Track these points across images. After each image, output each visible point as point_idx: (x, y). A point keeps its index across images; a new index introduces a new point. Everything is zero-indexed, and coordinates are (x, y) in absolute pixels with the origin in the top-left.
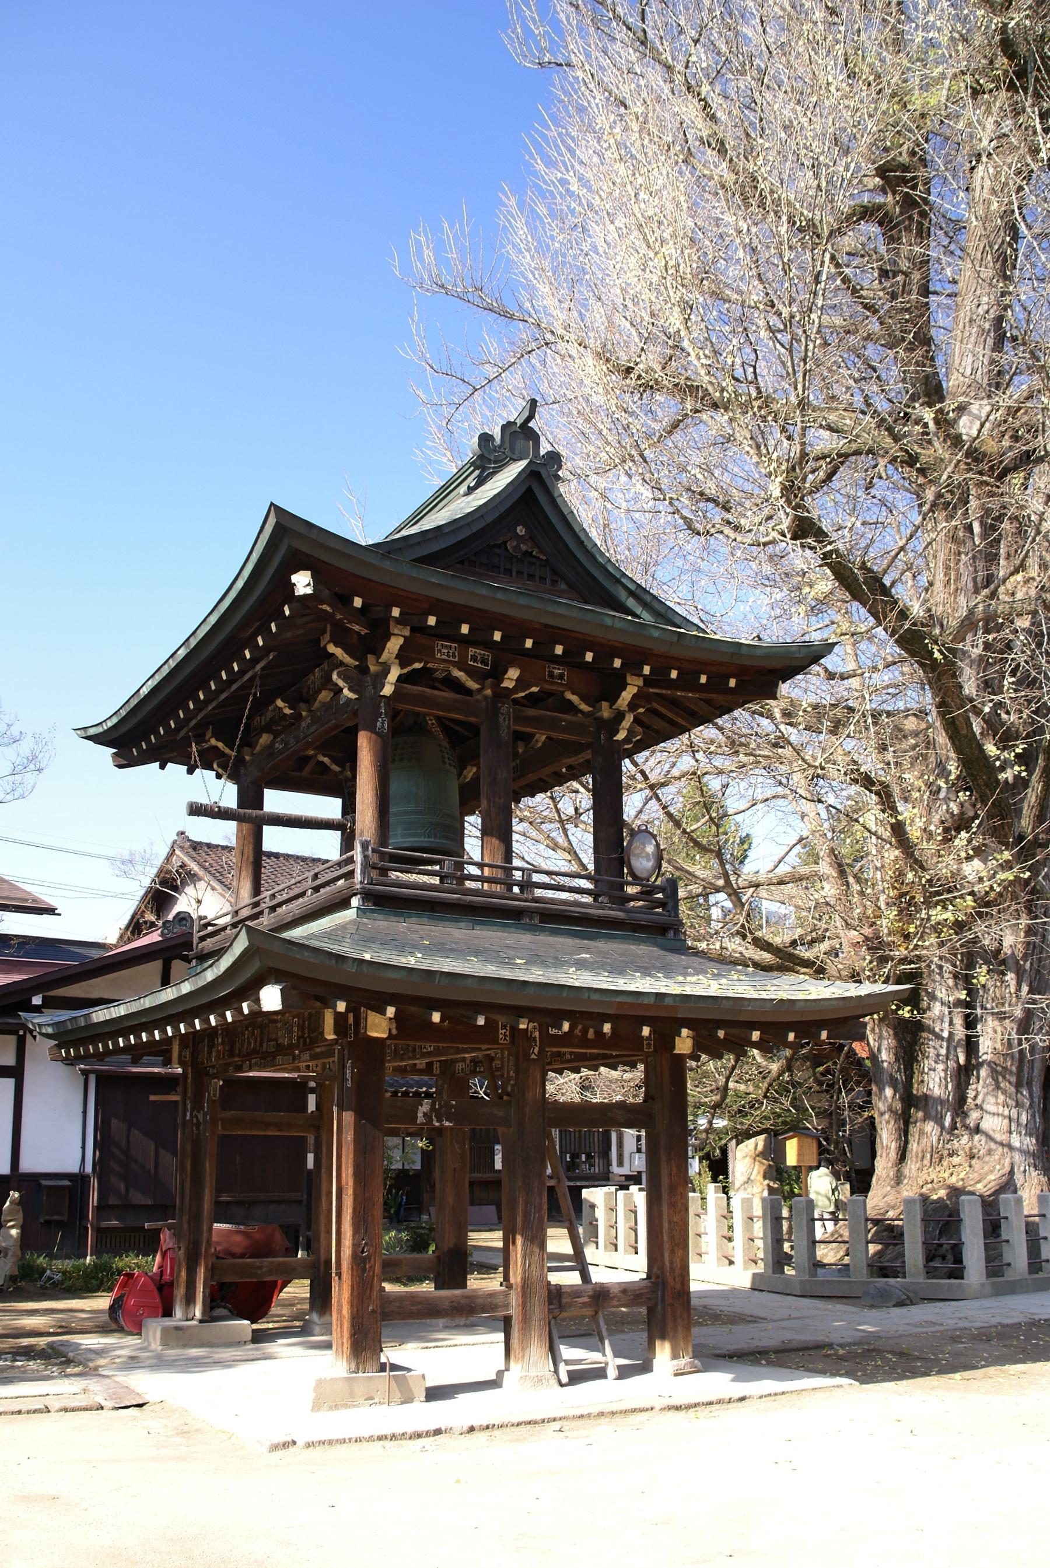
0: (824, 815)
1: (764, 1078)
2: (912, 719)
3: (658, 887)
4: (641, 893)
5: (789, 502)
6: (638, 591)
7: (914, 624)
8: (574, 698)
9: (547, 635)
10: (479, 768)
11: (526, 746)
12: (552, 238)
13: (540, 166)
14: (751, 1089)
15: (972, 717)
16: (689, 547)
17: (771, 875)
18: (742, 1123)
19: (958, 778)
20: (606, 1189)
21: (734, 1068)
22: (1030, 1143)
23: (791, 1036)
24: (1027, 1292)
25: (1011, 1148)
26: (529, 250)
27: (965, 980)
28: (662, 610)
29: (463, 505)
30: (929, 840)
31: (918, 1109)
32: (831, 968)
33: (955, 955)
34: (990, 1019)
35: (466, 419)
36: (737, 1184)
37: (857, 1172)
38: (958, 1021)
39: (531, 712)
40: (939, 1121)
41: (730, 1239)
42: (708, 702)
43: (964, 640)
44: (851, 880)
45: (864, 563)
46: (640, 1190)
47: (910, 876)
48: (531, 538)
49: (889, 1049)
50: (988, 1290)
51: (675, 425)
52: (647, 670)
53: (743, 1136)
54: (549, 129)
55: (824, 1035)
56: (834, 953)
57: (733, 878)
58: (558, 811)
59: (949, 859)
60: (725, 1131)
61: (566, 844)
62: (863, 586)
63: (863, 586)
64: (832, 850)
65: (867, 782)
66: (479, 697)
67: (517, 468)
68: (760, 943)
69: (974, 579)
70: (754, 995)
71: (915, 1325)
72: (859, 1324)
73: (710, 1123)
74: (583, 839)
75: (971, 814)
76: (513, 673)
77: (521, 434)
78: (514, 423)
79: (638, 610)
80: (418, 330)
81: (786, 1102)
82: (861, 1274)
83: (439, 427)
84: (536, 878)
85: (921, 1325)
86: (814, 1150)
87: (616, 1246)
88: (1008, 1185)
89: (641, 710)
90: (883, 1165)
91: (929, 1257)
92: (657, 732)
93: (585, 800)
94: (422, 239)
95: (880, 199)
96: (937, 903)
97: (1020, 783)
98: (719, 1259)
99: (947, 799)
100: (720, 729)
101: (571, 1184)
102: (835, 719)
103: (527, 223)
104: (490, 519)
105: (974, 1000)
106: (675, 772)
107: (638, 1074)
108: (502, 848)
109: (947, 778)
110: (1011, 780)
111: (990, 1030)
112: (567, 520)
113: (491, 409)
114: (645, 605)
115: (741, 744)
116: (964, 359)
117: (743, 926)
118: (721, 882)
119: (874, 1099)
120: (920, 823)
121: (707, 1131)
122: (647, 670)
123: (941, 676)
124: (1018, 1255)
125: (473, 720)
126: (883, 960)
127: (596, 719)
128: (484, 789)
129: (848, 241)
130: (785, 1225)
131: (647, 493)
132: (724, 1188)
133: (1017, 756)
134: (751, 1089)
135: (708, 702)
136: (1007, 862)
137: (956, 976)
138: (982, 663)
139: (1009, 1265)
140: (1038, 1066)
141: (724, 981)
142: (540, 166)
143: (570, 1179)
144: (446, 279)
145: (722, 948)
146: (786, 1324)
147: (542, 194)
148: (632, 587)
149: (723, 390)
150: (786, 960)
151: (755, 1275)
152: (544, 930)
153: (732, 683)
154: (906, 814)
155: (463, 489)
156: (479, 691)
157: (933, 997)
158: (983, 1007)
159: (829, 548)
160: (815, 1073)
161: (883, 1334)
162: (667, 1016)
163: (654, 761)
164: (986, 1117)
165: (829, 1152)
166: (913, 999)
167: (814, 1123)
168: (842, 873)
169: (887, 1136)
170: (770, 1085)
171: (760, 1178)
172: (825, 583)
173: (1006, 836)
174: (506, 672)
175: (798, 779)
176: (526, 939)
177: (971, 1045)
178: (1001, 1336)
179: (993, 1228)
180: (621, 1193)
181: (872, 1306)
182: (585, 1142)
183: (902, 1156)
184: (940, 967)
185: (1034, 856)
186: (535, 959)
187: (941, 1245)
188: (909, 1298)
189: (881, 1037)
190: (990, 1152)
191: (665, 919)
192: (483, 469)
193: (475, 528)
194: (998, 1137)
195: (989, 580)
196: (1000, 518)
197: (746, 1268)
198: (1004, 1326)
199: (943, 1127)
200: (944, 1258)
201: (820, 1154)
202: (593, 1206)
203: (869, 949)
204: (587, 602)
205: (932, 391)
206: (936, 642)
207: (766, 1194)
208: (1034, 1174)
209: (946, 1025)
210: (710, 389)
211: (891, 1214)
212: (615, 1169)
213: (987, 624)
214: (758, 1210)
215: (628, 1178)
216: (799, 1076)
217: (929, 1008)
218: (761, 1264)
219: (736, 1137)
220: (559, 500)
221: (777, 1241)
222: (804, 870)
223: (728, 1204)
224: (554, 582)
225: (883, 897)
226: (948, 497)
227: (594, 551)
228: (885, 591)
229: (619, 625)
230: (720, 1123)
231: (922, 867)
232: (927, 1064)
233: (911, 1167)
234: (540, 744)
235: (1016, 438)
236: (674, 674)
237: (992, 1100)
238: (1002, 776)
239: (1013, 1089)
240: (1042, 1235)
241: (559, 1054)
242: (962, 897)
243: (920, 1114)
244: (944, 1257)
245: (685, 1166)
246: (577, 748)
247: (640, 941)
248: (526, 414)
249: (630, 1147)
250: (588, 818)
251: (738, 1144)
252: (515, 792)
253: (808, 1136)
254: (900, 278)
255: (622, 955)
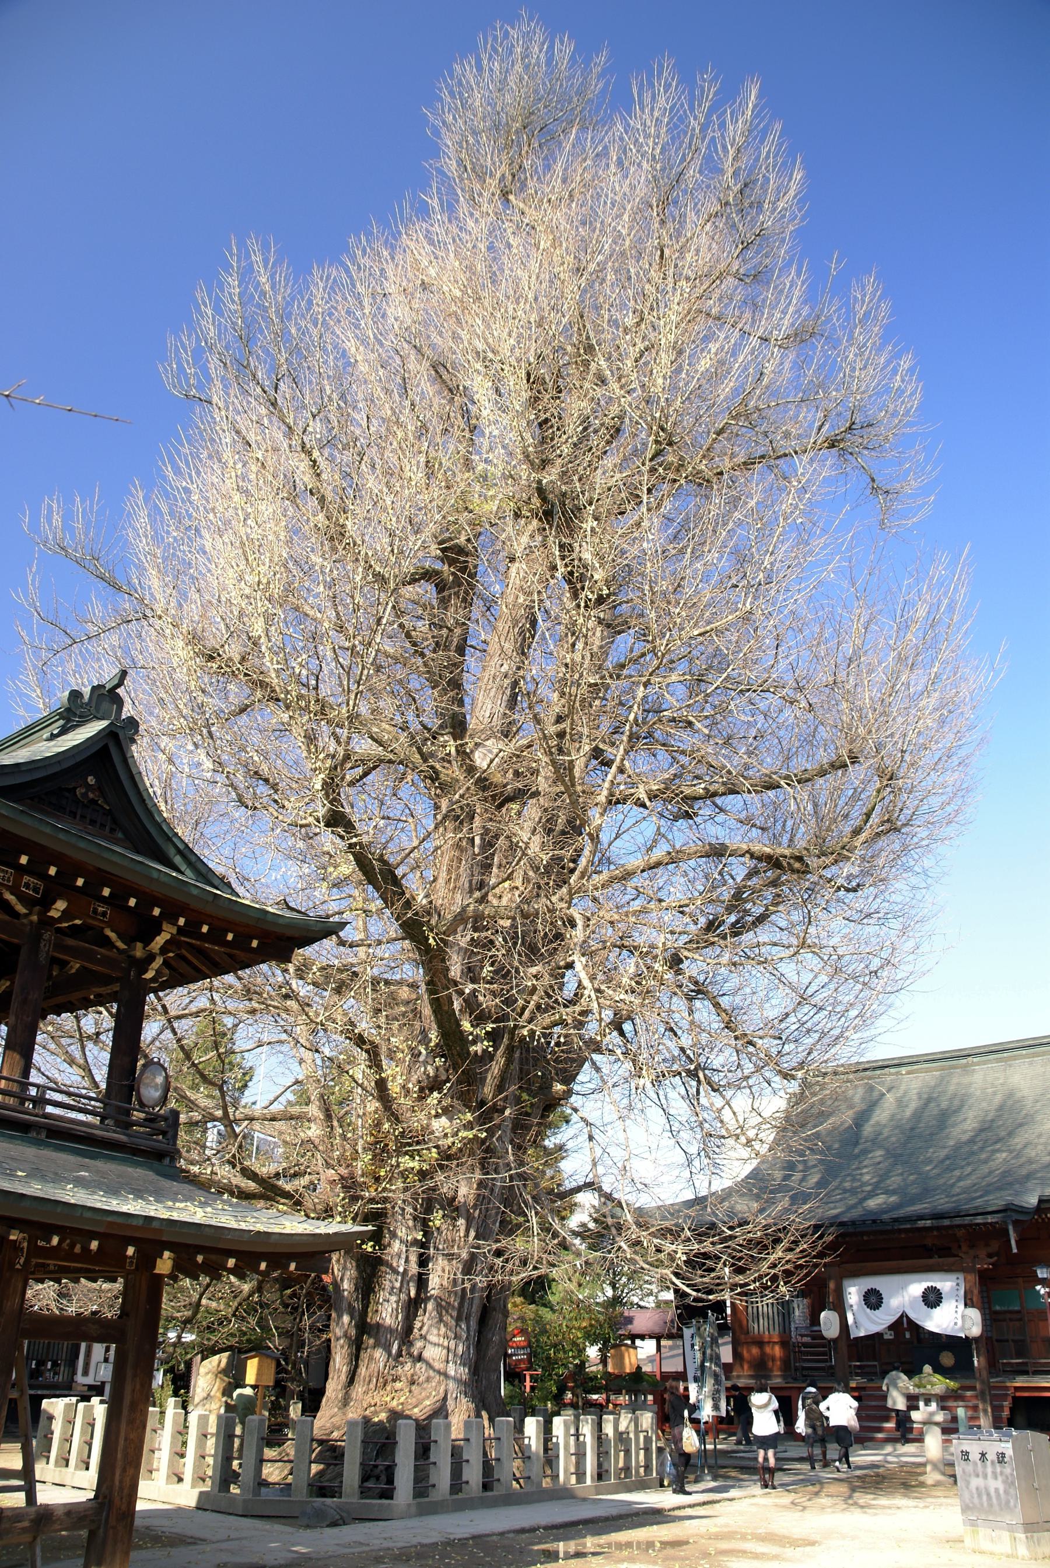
0: (319, 1062)
1: (235, 1297)
2: (406, 988)
3: (161, 1116)
4: (145, 1120)
5: (327, 795)
6: (186, 852)
7: (417, 914)
8: (113, 936)
9: (98, 877)
10: (13, 983)
11: (61, 970)
12: (168, 532)
13: (169, 473)
14: (222, 1307)
15: (454, 996)
16: (237, 815)
17: (266, 1111)
18: (209, 1339)
19: (437, 1045)
20: (67, 1400)
21: (208, 1285)
22: (463, 1372)
23: (263, 1266)
24: (447, 1512)
25: (446, 1375)
26: (146, 537)
27: (424, 1224)
28: (204, 871)
29: (43, 748)
30: (406, 1096)
31: (370, 1336)
32: (308, 1204)
33: (417, 1200)
34: (440, 1258)
35: (61, 663)
36: (197, 1400)
37: (311, 1391)
38: (413, 1259)
39: (70, 942)
40: (387, 1349)
41: (182, 1456)
42: (230, 956)
43: (455, 932)
44: (335, 1123)
45: (382, 855)
46: (102, 1402)
47: (386, 1126)
48: (99, 788)
49: (350, 1280)
50: (413, 1510)
51: (243, 710)
52: (182, 921)
53: (208, 1352)
54: (183, 445)
55: (293, 1266)
56: (312, 1187)
57: (231, 1110)
58: (79, 1028)
59: (422, 1116)
60: (192, 1345)
61: (82, 1062)
62: (379, 875)
63: (379, 875)
64: (322, 1096)
65: (360, 1041)
66: (25, 921)
67: (96, 727)
68: (248, 1173)
69: (470, 882)
70: (233, 1225)
71: (344, 1546)
72: (293, 1545)
73: (179, 1337)
74: (100, 1058)
75: (444, 1078)
76: (61, 905)
77: (107, 697)
78: (103, 686)
79: (183, 867)
80: (33, 581)
81: (253, 1321)
82: (301, 1494)
83: (35, 667)
84: (51, 1095)
85: (349, 1546)
86: (273, 1370)
87: (67, 1461)
88: (441, 1411)
89: (171, 955)
90: (333, 1387)
91: (365, 1478)
92: (181, 974)
93: (108, 1022)
94: (55, 506)
95: (438, 566)
96: (406, 1153)
97: (487, 1057)
98: (168, 1477)
99: (425, 1063)
100: (240, 979)
101: (32, 1392)
102: (342, 981)
103: (149, 515)
104: (65, 765)
105: (428, 1241)
106: (193, 1008)
107: (119, 1285)
108: (22, 1063)
109: (427, 1045)
110: (479, 1053)
111: (439, 1269)
112: (134, 779)
113: (85, 660)
114: (190, 864)
115: (256, 993)
116: (485, 707)
117: (234, 1156)
118: (219, 1113)
119: (333, 1324)
120: (400, 1080)
121: (174, 1345)
122: (182, 921)
123: (433, 959)
124: (442, 1477)
125: (16, 941)
126: (354, 1199)
127: (129, 957)
128: (14, 1006)
129: (408, 591)
130: (237, 1442)
131: (208, 764)
132: (184, 1402)
133: (487, 1033)
134: (222, 1307)
135: (230, 956)
136: (470, 1122)
137: (415, 1219)
138: (468, 953)
139: (434, 1486)
140: (476, 1302)
141: (209, 1209)
142: (169, 473)
143: (31, 1387)
144: (68, 542)
145: (212, 1172)
146: (224, 1546)
147: (167, 495)
148: (181, 846)
149: (288, 692)
150: (269, 1191)
151: (201, 1493)
152: (48, 1145)
153: (255, 944)
154: (389, 1072)
155: (46, 735)
156: (26, 915)
157: (394, 1235)
158: (436, 1248)
159: (354, 840)
160: (282, 1296)
161: (313, 1555)
162: (152, 1237)
163: (176, 998)
164: (429, 1346)
165: (286, 1372)
166: (376, 1237)
167: (276, 1343)
168: (328, 1117)
169: (339, 1360)
170: (240, 1304)
171: (219, 1394)
172: (347, 867)
173: (470, 1101)
174: (54, 903)
175: (301, 1031)
176: (30, 1152)
177: (422, 1282)
178: (419, 1556)
179: (423, 1450)
180: (81, 1405)
181: (308, 1527)
182: (48, 1356)
183: (351, 1380)
184: (403, 1210)
185: (491, 1120)
186: (35, 1173)
187: (376, 1466)
188: (342, 1518)
189: (345, 1268)
190: (428, 1380)
191: (164, 1146)
192: (68, 720)
193: (50, 771)
194: (437, 1365)
195: (481, 885)
196: (497, 837)
197: (193, 1486)
198: (423, 1545)
199: (390, 1354)
200: (378, 1478)
201: (278, 1373)
202: (51, 1418)
203: (343, 1187)
204: (138, 852)
205: (458, 726)
206: (432, 930)
207: (222, 1411)
208: (464, 1400)
209: (402, 1261)
210: (277, 689)
211: (335, 1435)
212: (80, 1378)
213: (475, 921)
214: (212, 1428)
215: (91, 1387)
216: (267, 1296)
217: (389, 1245)
218: (209, 1482)
219: (202, 1352)
220: (130, 761)
221: (226, 1458)
222: (296, 1110)
223: (186, 1420)
224: (112, 830)
225: (361, 1142)
226: (459, 812)
227: (153, 809)
228: (396, 881)
229: (163, 879)
230: (188, 1337)
231: (397, 1119)
232: (382, 1296)
233: (358, 1389)
234: (73, 971)
235: (517, 774)
236: (205, 929)
237: (435, 1331)
238: (473, 1049)
239: (453, 1323)
240: (465, 1458)
241: (44, 1265)
242: (428, 1149)
243: (371, 1341)
244: (378, 1478)
245: (151, 1377)
246: (107, 980)
247: (137, 1164)
248: (116, 682)
249: (99, 1362)
250: (108, 1039)
251: (203, 1360)
252: (43, 1010)
253: (268, 1356)
254: (445, 632)
255: (119, 1176)
